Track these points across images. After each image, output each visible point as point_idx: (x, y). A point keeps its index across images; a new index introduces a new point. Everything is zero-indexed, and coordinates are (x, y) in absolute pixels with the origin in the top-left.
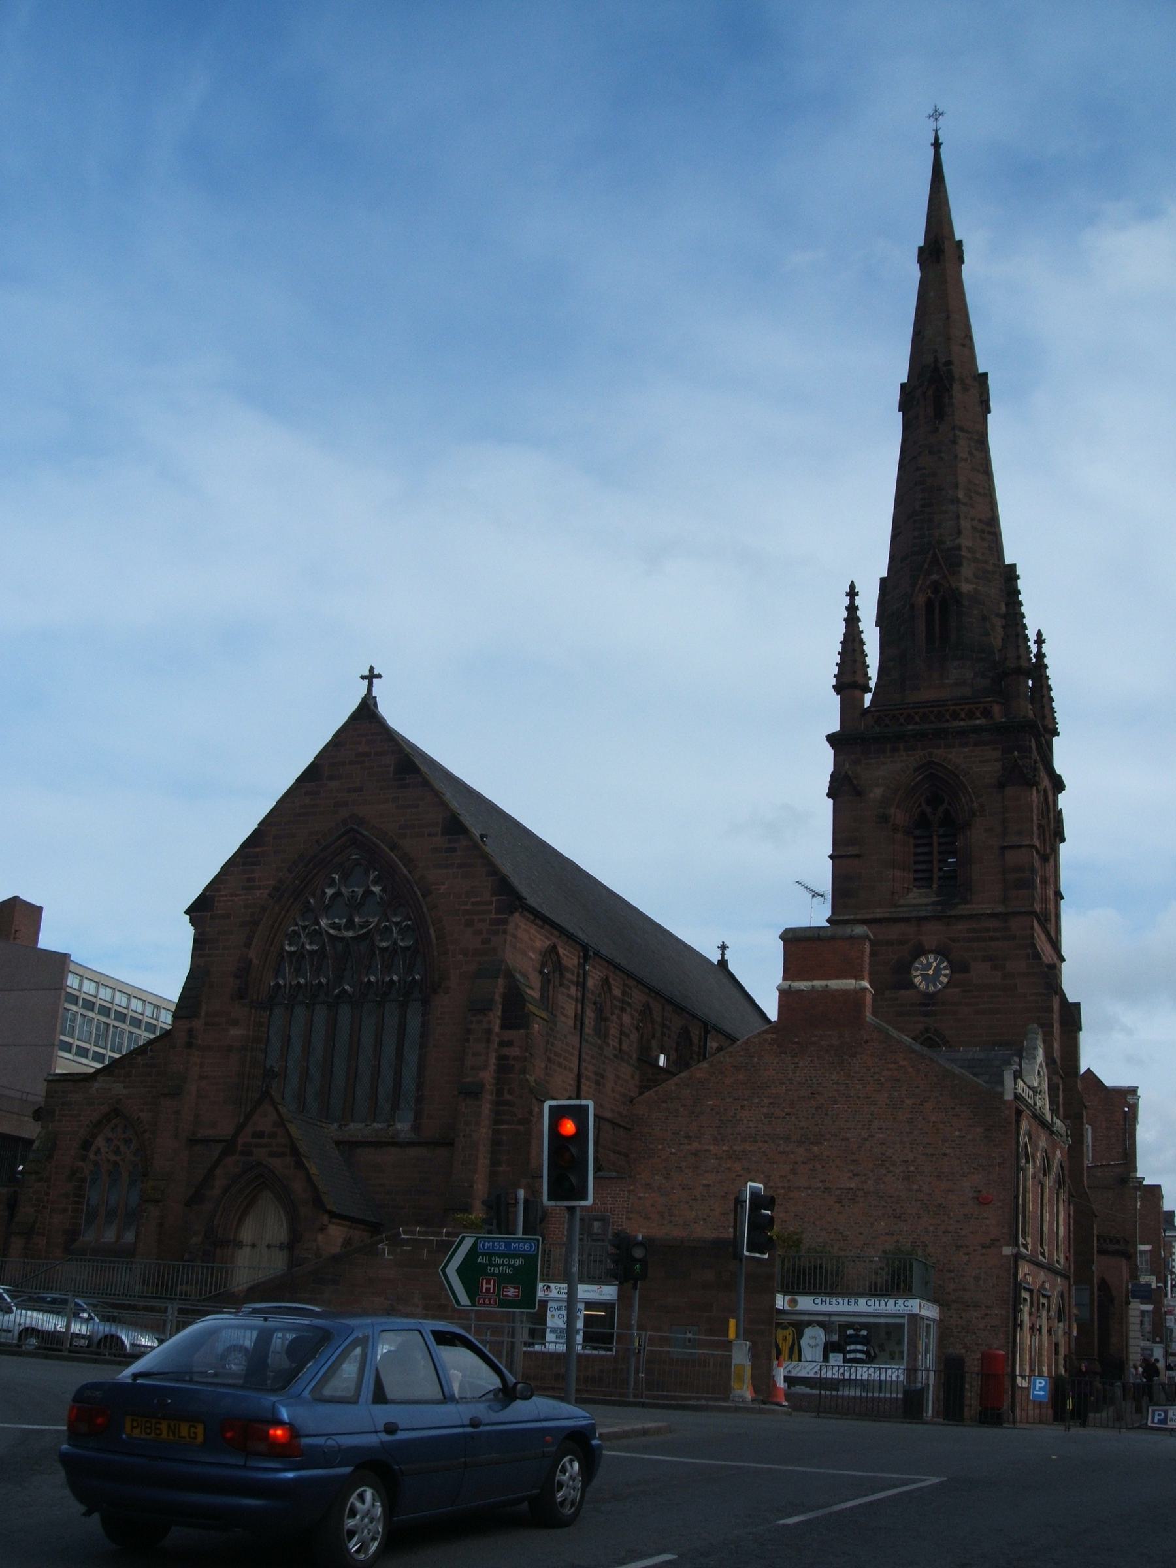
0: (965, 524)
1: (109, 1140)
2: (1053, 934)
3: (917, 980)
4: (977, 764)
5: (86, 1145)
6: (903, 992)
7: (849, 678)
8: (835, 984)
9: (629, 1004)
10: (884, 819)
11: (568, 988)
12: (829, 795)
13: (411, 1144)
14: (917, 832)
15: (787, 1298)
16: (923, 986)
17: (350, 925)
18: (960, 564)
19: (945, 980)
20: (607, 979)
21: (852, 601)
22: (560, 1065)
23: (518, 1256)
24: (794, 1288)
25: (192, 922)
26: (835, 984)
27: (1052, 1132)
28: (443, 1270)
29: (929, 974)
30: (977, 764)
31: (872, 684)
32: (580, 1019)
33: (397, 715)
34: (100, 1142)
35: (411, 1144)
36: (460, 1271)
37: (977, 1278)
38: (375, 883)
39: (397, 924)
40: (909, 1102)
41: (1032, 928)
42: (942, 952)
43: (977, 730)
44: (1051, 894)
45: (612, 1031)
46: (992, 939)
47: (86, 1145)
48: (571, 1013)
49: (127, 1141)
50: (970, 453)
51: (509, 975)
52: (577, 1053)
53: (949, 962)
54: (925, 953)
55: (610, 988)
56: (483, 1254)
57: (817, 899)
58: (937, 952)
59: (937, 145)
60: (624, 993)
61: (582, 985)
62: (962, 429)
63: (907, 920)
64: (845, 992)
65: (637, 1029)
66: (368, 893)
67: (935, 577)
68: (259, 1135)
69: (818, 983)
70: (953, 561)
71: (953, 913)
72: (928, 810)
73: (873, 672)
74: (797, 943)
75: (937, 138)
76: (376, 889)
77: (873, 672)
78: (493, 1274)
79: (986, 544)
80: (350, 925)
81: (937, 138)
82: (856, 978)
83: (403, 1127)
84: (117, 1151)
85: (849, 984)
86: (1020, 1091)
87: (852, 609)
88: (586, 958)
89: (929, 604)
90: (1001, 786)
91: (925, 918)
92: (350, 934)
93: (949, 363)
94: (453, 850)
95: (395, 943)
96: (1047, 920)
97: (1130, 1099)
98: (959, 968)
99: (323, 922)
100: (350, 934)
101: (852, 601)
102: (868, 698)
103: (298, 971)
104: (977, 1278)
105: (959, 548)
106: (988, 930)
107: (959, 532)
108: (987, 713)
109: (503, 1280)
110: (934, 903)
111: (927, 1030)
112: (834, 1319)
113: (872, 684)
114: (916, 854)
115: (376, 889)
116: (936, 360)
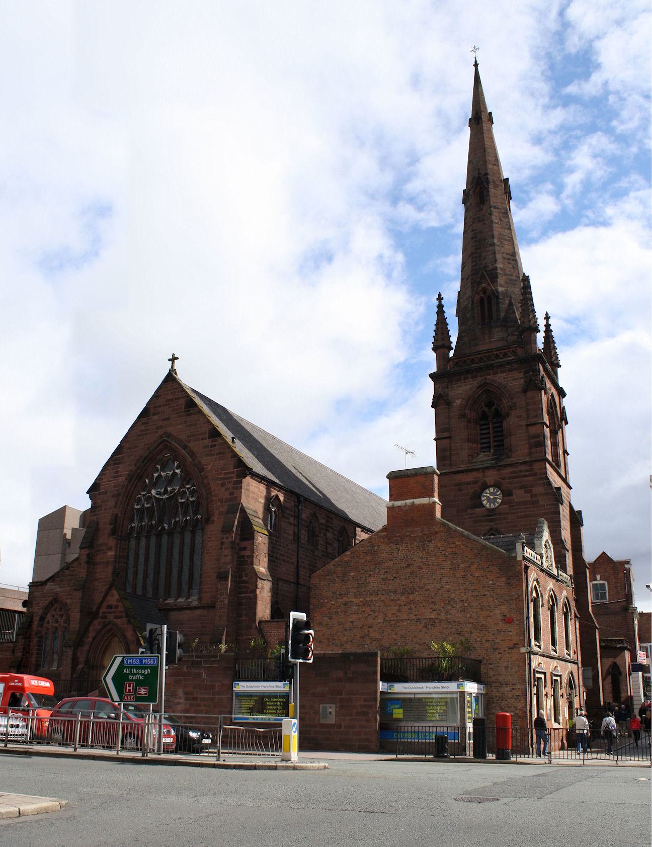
0: (499, 256)
1: (53, 616)
2: (563, 474)
3: (484, 503)
4: (511, 380)
5: (42, 619)
6: (477, 510)
7: (441, 343)
8: (418, 501)
9: (332, 528)
10: (464, 416)
11: (288, 519)
12: (432, 406)
13: (196, 608)
14: (481, 422)
15: (386, 684)
16: (488, 506)
17: (166, 492)
18: (497, 277)
19: (500, 501)
20: (315, 513)
21: (440, 302)
22: (284, 561)
23: (146, 668)
24: (389, 678)
25: (90, 497)
26: (418, 501)
27: (558, 581)
28: (104, 679)
29: (491, 498)
30: (511, 380)
31: (453, 345)
32: (297, 537)
33: (186, 379)
34: (49, 617)
35: (196, 608)
36: (114, 679)
37: (507, 667)
38: (177, 468)
39: (188, 489)
40: (462, 566)
41: (546, 468)
42: (496, 485)
43: (509, 363)
44: (561, 452)
45: (321, 542)
46: (524, 476)
47: (42, 619)
48: (291, 532)
49: (62, 616)
50: (500, 219)
51: (243, 510)
52: (295, 554)
53: (502, 491)
54: (488, 487)
55: (317, 518)
56: (127, 667)
57: (409, 454)
58: (494, 486)
59: (476, 65)
60: (327, 521)
61: (297, 517)
62: (495, 208)
63: (478, 470)
64: (424, 505)
65: (338, 540)
66: (175, 474)
67: (483, 285)
68: (110, 607)
69: (409, 501)
70: (493, 277)
71: (502, 463)
72: (486, 409)
73: (454, 339)
74: (400, 481)
75: (476, 61)
76: (178, 471)
77: (454, 339)
78: (132, 680)
79: (510, 266)
80: (166, 492)
81: (476, 61)
82: (429, 497)
83: (194, 600)
84: (57, 621)
85: (425, 501)
86: (526, 555)
87: (440, 306)
88: (299, 502)
89: (482, 300)
90: (525, 391)
91: (487, 468)
92: (166, 496)
93: (486, 174)
94: (215, 446)
95: (188, 499)
96: (558, 465)
97: (627, 566)
98: (507, 494)
99: (153, 492)
100: (166, 496)
101: (440, 302)
102: (451, 354)
103: (141, 519)
104: (507, 667)
105: (496, 268)
106: (521, 471)
107: (496, 261)
108: (514, 353)
109: (139, 683)
110: (493, 459)
111: (491, 529)
112: (434, 696)
113: (453, 345)
114: (482, 434)
115: (178, 471)
116: (479, 173)
